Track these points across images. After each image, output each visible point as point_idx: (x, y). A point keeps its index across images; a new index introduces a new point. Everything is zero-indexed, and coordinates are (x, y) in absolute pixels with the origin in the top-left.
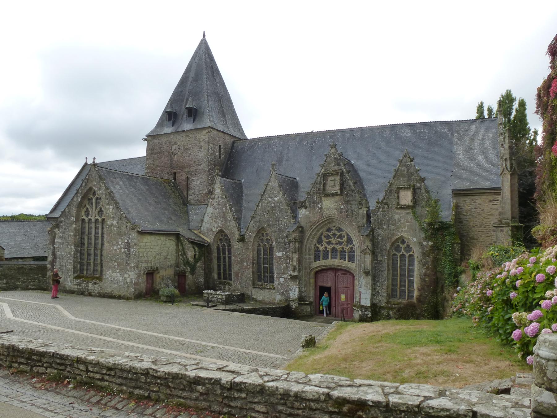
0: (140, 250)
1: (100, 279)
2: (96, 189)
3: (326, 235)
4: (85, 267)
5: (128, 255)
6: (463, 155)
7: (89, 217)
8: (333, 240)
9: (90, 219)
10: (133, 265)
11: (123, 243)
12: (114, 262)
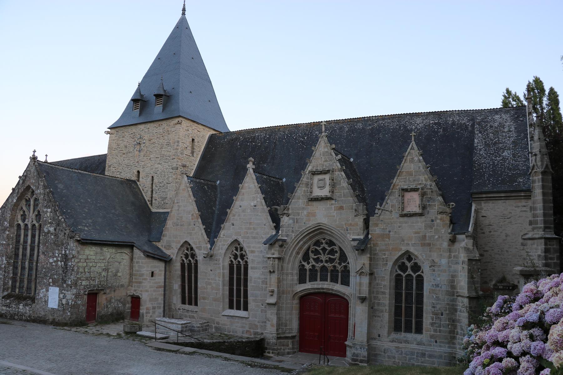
0: (80, 264)
1: (33, 300)
2: (34, 188)
3: (314, 250)
4: (18, 284)
5: (65, 269)
6: (485, 150)
7: (25, 223)
8: (323, 257)
9: (26, 225)
10: (70, 283)
11: (60, 255)
12: (49, 279)
